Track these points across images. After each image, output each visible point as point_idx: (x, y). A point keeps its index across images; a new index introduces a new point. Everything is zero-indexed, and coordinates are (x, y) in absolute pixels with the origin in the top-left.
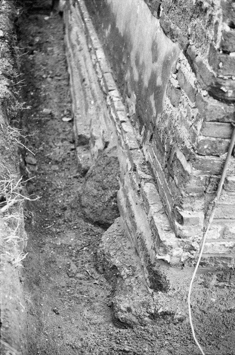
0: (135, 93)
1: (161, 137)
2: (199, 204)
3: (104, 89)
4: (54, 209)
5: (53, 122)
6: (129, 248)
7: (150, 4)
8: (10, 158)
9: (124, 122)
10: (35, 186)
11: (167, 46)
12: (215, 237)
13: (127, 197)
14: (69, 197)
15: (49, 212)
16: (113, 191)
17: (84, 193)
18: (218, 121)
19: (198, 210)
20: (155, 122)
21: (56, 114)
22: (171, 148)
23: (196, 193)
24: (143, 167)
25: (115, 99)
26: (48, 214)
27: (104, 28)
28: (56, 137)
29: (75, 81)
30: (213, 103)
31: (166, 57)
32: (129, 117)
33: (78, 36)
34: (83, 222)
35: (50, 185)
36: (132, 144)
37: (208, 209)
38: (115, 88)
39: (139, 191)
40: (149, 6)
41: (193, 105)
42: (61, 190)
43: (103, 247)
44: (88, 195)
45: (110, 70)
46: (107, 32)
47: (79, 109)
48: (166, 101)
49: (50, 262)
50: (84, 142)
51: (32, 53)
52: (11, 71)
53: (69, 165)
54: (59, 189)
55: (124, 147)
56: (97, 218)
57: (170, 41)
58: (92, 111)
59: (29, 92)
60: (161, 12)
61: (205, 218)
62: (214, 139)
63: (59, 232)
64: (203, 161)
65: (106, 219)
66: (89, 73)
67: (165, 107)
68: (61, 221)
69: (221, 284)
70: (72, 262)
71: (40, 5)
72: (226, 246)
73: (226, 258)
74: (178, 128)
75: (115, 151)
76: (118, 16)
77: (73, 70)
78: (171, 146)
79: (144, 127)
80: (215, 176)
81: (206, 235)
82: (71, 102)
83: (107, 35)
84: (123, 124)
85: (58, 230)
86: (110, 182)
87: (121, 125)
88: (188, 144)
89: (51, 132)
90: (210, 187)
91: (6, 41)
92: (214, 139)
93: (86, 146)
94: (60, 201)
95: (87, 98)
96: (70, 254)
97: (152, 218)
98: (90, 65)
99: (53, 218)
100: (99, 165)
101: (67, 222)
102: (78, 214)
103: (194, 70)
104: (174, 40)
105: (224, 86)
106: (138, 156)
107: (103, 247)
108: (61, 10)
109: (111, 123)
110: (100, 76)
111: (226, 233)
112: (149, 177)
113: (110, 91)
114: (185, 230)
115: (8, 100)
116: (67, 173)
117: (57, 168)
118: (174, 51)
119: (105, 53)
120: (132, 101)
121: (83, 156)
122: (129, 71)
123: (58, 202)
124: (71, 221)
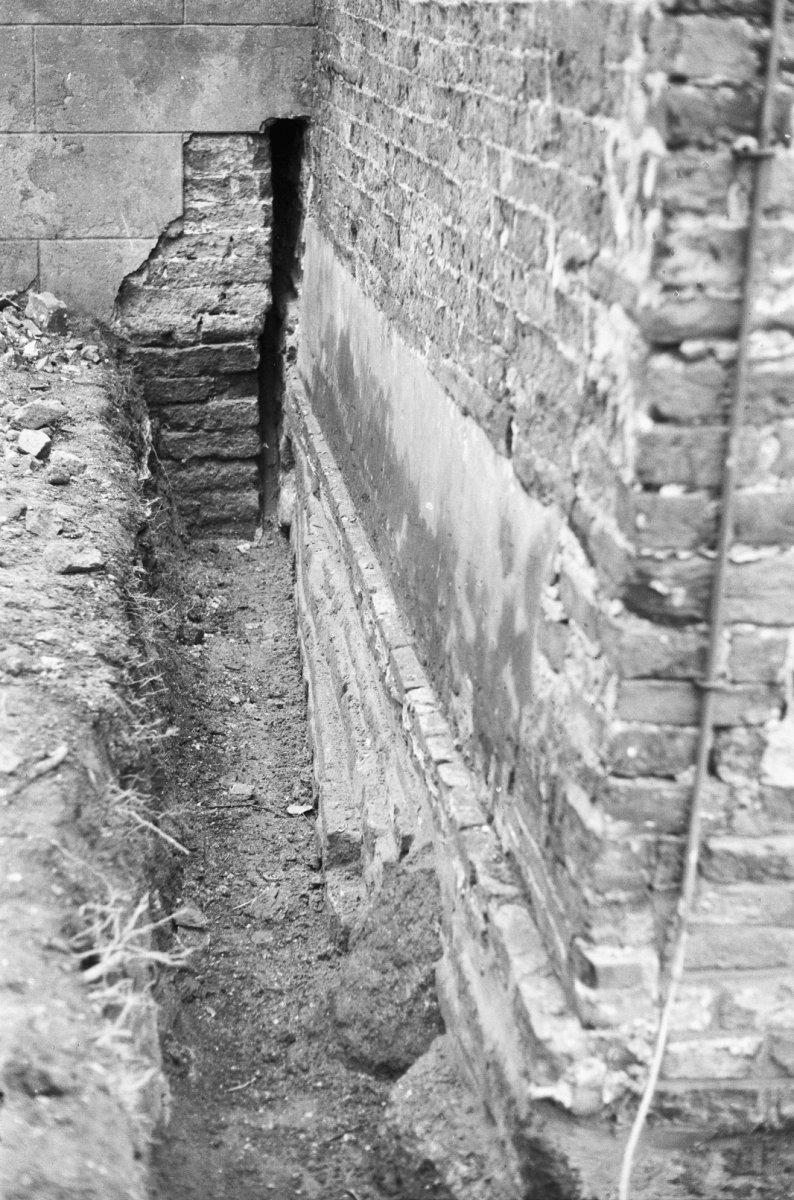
0: (471, 676)
1: (533, 768)
2: (640, 924)
3: (394, 690)
4: (258, 1042)
5: (257, 818)
6: (470, 1111)
7: (488, 426)
8: (114, 859)
9: (445, 761)
10: (202, 982)
11: (535, 519)
12: (696, 1025)
13: (461, 966)
14: (304, 1009)
15: (242, 1051)
16: (426, 967)
17: (343, 984)
18: (656, 676)
19: (637, 945)
20: (518, 733)
21: (269, 797)
22: (554, 784)
23: (625, 889)
24: (494, 866)
25: (419, 709)
26: (240, 1055)
27: (391, 530)
28: (267, 859)
29: (319, 697)
30: (638, 629)
31: (534, 548)
32: (458, 748)
33: (326, 572)
34: (343, 1071)
35: (247, 980)
36: (467, 813)
37: (666, 939)
38: (425, 682)
39: (485, 933)
40: (488, 432)
41: (594, 649)
42: (281, 993)
43: (395, 1116)
44: (354, 989)
45: (410, 640)
46: (400, 538)
47: (331, 766)
48: (540, 664)
49: (240, 1173)
50: (345, 853)
51: (200, 640)
52: (121, 649)
53: (307, 926)
54: (275, 992)
55: (447, 830)
56: (381, 1053)
57: (537, 505)
58: (366, 765)
59: (190, 741)
60: (515, 438)
61: (662, 968)
62: (654, 729)
63: (270, 1099)
64: (632, 794)
65: (409, 1051)
66: (358, 666)
67: (537, 684)
68: (277, 1072)
69: (739, 1182)
70: (306, 1174)
71: (223, 508)
72: (735, 1050)
73: (741, 1093)
74: (567, 725)
75: (428, 857)
76: (422, 487)
77: (319, 676)
78: (555, 778)
79: (493, 758)
80: (672, 839)
81: (666, 1018)
82: (310, 761)
83: (398, 549)
84: (442, 768)
85: (268, 1094)
86: (417, 942)
87: (436, 772)
88: (591, 759)
89: (252, 846)
90: (662, 873)
91: (111, 576)
92: (654, 729)
93: (354, 865)
94: (276, 1022)
95: (355, 735)
96: (303, 1153)
97: (517, 990)
98: (359, 639)
99: (253, 1064)
100: (385, 903)
101: (295, 1074)
102: (326, 1049)
103: (592, 562)
104: (545, 500)
105: (659, 579)
106: (482, 841)
107: (395, 1116)
108: (286, 519)
109: (418, 784)
110: (384, 661)
111: (726, 1009)
112: (511, 890)
113: (407, 691)
114: (604, 1002)
115: (112, 716)
116: (298, 951)
117: (268, 937)
118: (548, 529)
119: (396, 598)
120: (463, 704)
121: (342, 893)
122: (452, 623)
123: (271, 1023)
124: (306, 1071)
